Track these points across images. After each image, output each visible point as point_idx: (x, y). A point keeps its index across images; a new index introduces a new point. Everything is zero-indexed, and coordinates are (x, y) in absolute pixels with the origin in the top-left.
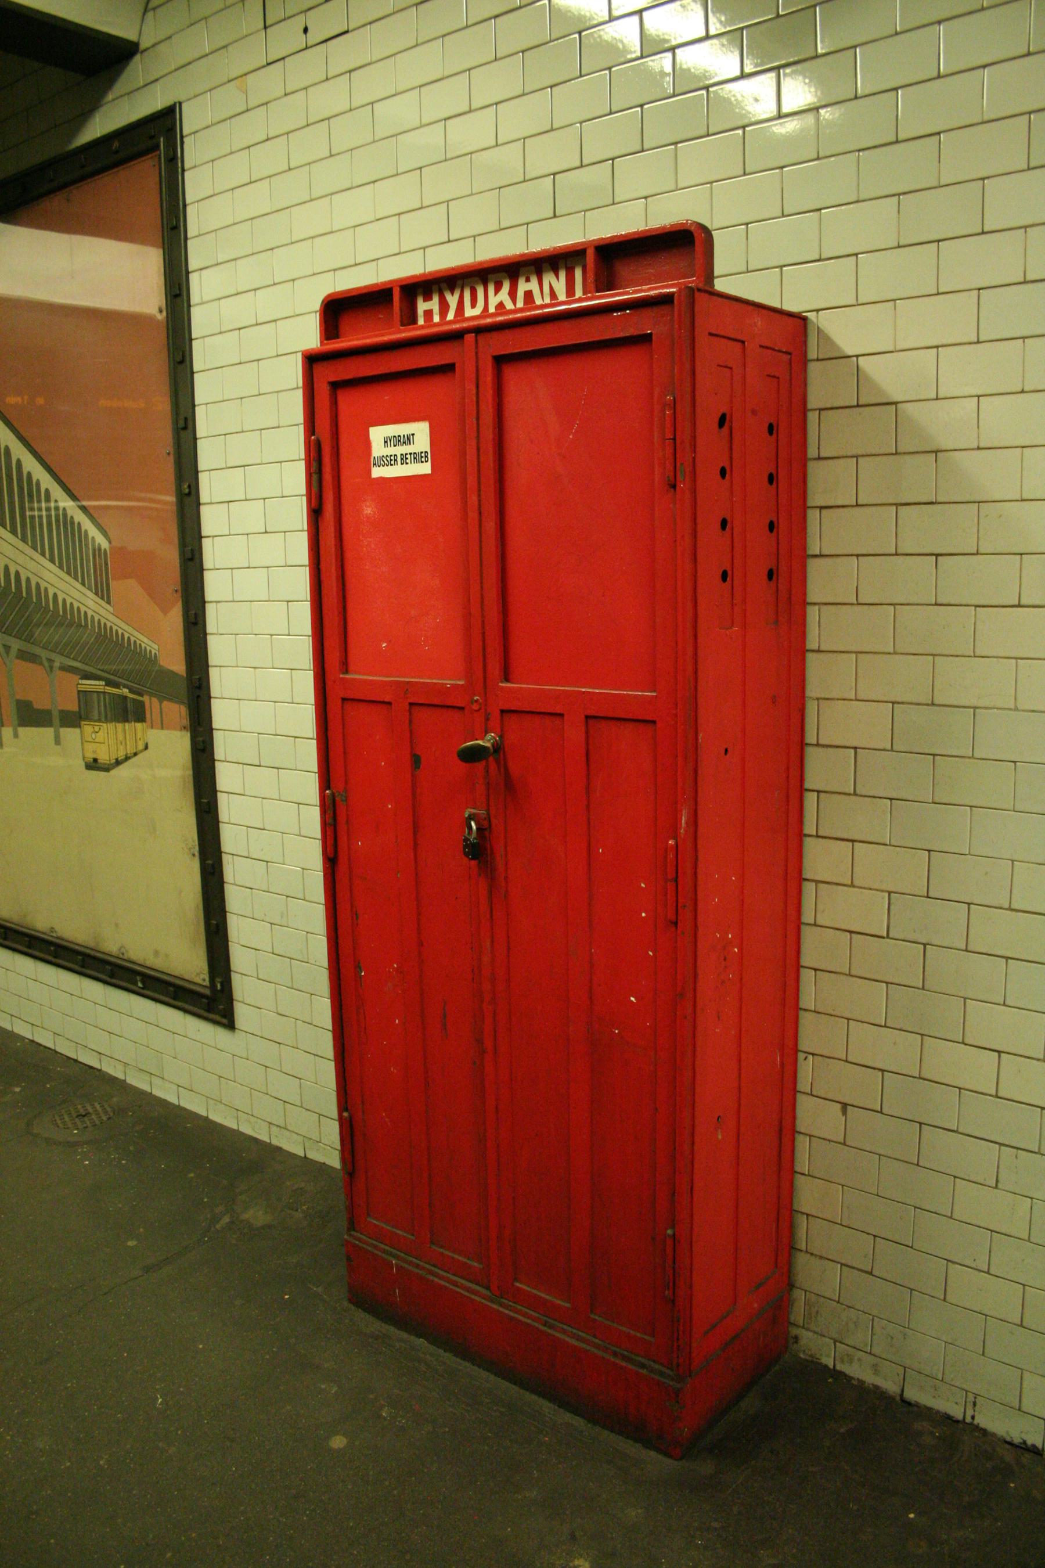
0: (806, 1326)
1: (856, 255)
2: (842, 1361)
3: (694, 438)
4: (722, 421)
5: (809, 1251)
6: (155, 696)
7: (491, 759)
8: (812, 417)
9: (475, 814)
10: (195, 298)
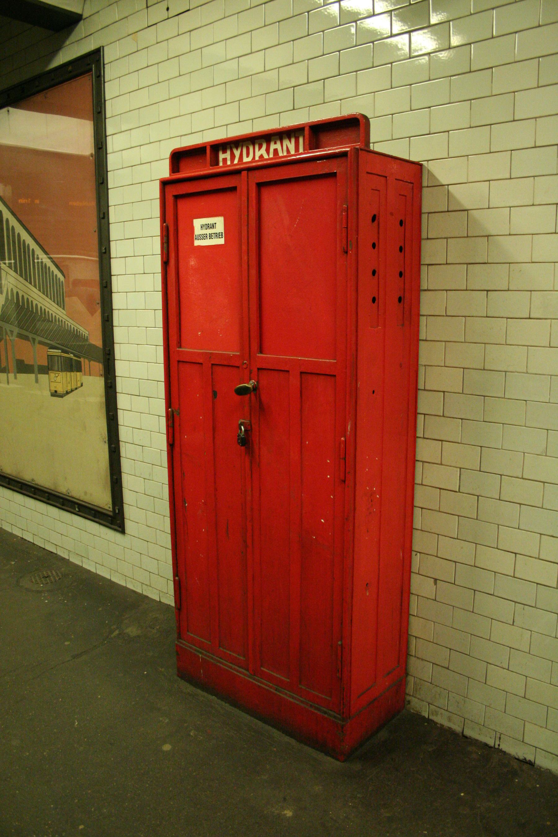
0: (414, 696)
1: (448, 131)
2: (433, 714)
3: (357, 227)
4: (374, 218)
5: (416, 656)
6: (87, 358)
7: (252, 393)
8: (424, 217)
9: (243, 422)
10: (109, 150)
